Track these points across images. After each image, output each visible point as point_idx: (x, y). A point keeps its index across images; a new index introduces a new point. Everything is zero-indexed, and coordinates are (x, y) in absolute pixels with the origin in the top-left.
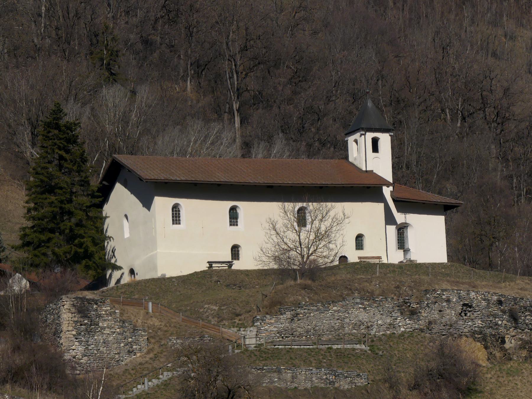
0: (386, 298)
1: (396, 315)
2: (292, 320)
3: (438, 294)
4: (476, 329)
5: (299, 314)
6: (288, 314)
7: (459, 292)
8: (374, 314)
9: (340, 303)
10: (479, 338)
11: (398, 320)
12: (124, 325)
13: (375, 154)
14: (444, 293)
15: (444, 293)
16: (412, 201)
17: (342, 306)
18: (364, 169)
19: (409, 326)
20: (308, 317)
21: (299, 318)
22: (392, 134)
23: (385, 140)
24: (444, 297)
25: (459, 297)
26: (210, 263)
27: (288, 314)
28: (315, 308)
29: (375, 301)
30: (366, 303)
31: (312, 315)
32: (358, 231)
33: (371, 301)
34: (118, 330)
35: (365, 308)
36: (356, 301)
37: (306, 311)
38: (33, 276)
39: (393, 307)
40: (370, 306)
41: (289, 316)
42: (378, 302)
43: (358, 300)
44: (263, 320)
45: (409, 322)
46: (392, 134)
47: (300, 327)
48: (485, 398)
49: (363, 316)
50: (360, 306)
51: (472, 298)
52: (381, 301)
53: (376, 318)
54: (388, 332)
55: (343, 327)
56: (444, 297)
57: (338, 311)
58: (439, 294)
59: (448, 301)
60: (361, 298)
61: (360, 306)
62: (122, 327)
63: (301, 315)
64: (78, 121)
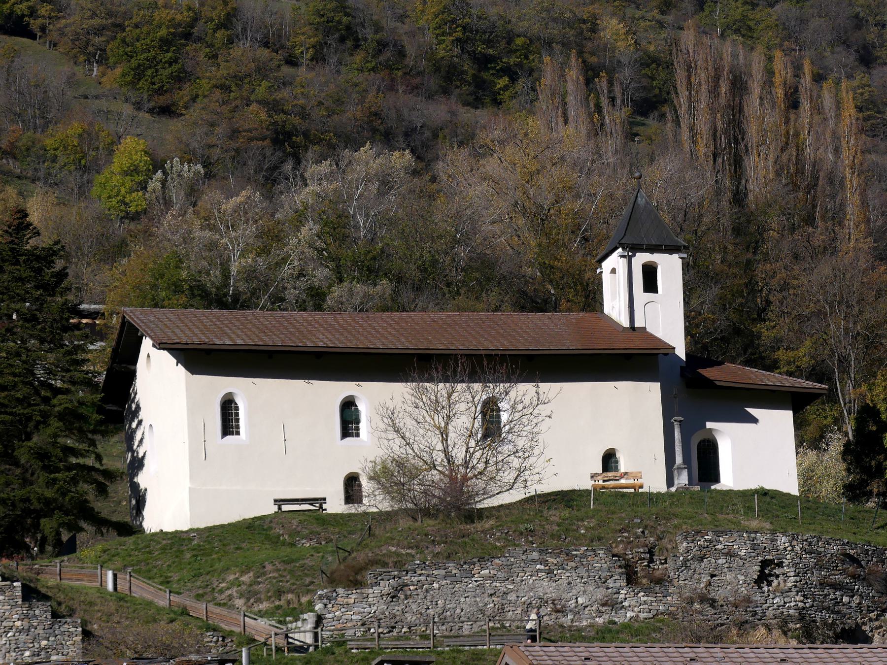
0: (594, 551)
1: (618, 585)
2: (393, 597)
3: (706, 541)
4: (792, 612)
5: (408, 585)
6: (385, 587)
7: (753, 535)
8: (569, 583)
9: (497, 561)
10: (796, 629)
11: (621, 596)
12: (31, 612)
13: (650, 296)
14: (721, 539)
15: (721, 539)
16: (744, 386)
17: (501, 568)
18: (626, 323)
19: (646, 606)
20: (427, 591)
21: (409, 593)
22: (685, 256)
23: (670, 268)
24: (720, 547)
25: (754, 547)
26: (279, 502)
27: (385, 587)
28: (443, 572)
29: (570, 556)
30: (551, 560)
31: (436, 585)
32: (591, 434)
33: (563, 556)
34: (18, 623)
35: (549, 572)
36: (530, 558)
37: (423, 578)
38: (113, 566)
39: (609, 570)
40: (561, 566)
41: (386, 590)
42: (577, 559)
43: (535, 555)
44: (329, 599)
45: (645, 598)
46: (685, 256)
47: (411, 611)
48: (263, 664)
49: (547, 588)
50: (538, 567)
51: (781, 547)
52: (583, 556)
53: (574, 592)
54: (600, 621)
55: (502, 610)
56: (720, 547)
57: (493, 578)
58: (711, 541)
59: (730, 554)
60: (541, 552)
61: (538, 567)
62: (27, 616)
63: (412, 588)
64: (59, 246)
